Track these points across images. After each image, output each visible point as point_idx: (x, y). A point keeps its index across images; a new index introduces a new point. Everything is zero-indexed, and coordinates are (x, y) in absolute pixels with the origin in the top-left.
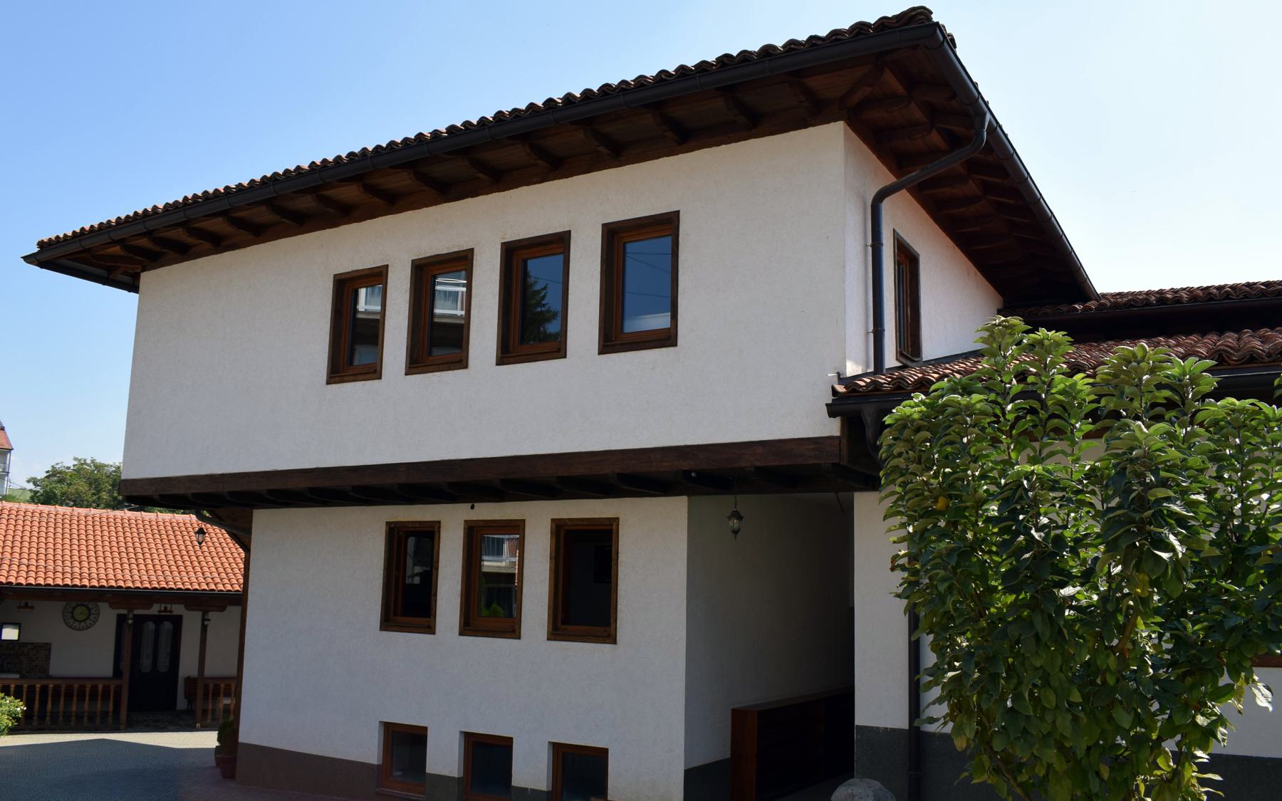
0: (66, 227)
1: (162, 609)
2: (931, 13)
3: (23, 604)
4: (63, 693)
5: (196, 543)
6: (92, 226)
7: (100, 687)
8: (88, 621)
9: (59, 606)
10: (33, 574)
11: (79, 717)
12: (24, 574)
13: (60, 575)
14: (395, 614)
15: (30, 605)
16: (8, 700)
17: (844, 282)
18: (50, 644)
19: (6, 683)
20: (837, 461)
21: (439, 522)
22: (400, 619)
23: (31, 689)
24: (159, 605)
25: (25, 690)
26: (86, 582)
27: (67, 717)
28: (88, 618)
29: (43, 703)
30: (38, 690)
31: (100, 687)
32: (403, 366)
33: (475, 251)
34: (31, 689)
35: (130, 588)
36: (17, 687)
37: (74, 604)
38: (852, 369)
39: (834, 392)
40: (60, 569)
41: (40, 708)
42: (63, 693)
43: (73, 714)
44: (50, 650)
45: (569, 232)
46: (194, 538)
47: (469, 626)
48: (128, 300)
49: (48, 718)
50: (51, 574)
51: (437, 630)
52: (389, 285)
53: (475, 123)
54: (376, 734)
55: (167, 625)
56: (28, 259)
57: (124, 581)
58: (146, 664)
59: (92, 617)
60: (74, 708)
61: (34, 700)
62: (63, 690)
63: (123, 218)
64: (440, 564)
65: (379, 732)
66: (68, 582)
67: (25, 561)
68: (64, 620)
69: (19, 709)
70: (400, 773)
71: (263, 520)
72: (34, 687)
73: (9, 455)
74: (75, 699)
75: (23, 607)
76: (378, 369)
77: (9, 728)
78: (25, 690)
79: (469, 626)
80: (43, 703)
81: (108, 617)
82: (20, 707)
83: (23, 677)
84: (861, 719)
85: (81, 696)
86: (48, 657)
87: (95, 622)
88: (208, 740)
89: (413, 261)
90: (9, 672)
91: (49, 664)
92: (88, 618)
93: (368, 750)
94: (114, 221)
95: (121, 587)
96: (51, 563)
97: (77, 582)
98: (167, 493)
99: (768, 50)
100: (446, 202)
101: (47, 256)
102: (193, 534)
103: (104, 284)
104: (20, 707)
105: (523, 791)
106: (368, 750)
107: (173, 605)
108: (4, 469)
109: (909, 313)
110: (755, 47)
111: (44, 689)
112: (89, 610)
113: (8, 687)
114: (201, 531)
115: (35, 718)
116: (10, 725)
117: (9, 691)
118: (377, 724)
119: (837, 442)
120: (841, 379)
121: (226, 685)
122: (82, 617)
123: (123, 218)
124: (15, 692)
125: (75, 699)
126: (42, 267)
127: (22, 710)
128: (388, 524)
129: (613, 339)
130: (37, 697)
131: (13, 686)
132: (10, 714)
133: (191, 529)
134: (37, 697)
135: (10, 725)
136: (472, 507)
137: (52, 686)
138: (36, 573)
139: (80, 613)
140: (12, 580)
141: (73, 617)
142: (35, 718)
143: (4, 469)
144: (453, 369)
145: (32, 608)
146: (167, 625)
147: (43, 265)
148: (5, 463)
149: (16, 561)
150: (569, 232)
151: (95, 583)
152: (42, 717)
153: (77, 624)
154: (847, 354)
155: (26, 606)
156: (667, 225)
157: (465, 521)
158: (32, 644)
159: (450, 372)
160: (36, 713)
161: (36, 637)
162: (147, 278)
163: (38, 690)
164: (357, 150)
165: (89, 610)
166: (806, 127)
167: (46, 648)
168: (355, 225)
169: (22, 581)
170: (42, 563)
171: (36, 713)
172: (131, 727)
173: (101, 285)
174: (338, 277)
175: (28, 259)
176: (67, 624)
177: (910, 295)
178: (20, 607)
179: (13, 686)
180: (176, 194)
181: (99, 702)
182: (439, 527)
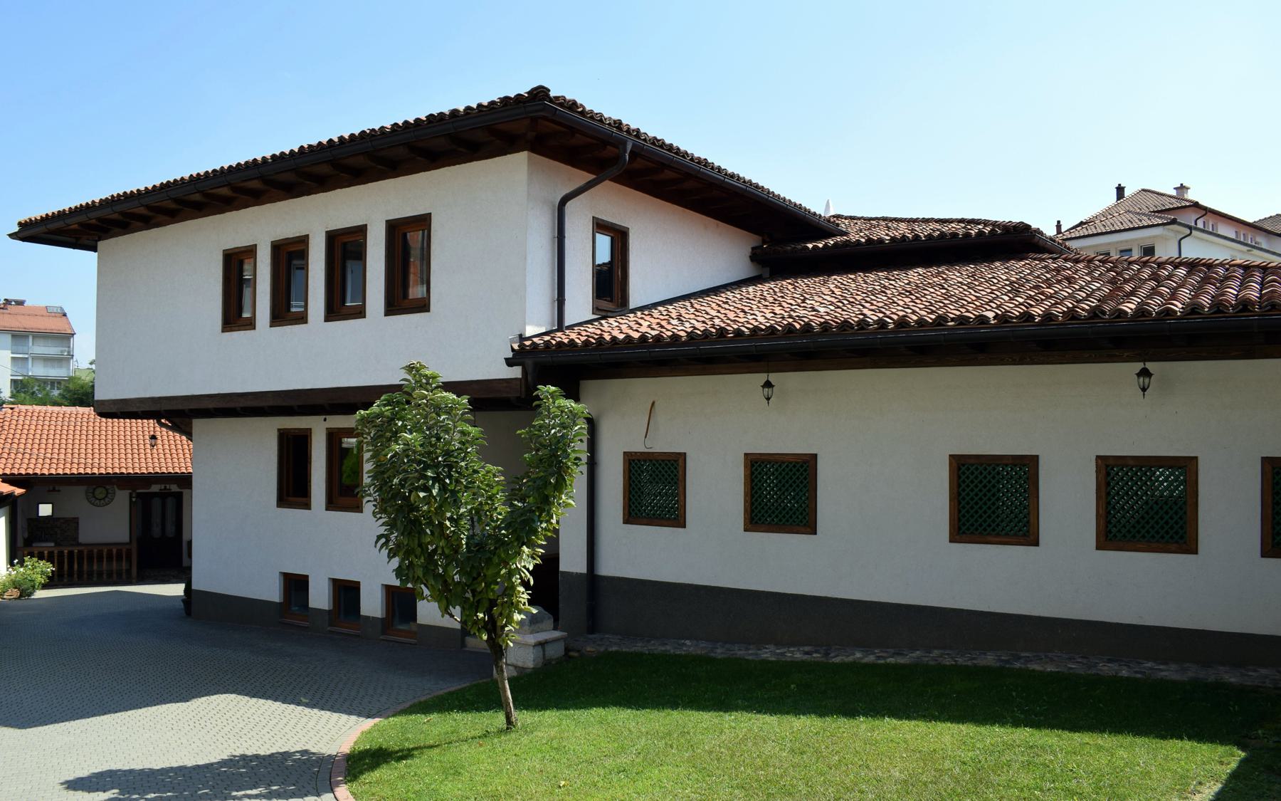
0: (37, 212)
1: (163, 488)
2: (549, 91)
3: (51, 488)
4: (105, 556)
5: (148, 446)
6: (53, 213)
7: (115, 551)
8: (106, 500)
9: (81, 489)
10: (54, 466)
11: (100, 574)
12: (47, 466)
13: (75, 466)
14: (288, 496)
15: (57, 489)
16: (42, 563)
17: (525, 269)
18: (78, 518)
19: (41, 550)
20: (519, 395)
21: (311, 429)
22: (291, 499)
23: (61, 554)
24: (765, 375)
25: (56, 555)
26: (95, 471)
27: (90, 574)
28: (106, 497)
29: (80, 565)
30: (66, 554)
31: (115, 551)
32: (269, 320)
33: (310, 237)
34: (61, 554)
35: (130, 473)
36: (49, 553)
37: (94, 487)
38: (530, 331)
39: (513, 350)
40: (75, 460)
41: (68, 569)
42: (105, 556)
43: (105, 572)
44: (78, 523)
45: (366, 225)
46: (148, 442)
47: (332, 504)
48: (92, 256)
49: (76, 576)
50: (68, 465)
51: (312, 507)
52: (258, 260)
53: (287, 153)
54: (278, 582)
55: (170, 502)
56: (12, 236)
57: (126, 468)
58: (156, 531)
59: (109, 496)
60: (95, 567)
61: (64, 562)
62: (85, 553)
63: (73, 208)
64: (312, 460)
65: (329, 585)
66: (82, 471)
67: (49, 455)
68: (87, 499)
69: (49, 570)
70: (297, 608)
71: (198, 425)
72: (62, 552)
73: (72, 339)
74: (95, 560)
75: (52, 491)
76: (253, 322)
77: (43, 584)
78: (56, 555)
79: (332, 504)
80: (80, 565)
81: (122, 498)
82: (49, 568)
83: (57, 544)
84: (563, 568)
85: (100, 559)
86: (77, 528)
87: (112, 499)
88: (177, 590)
89: (272, 242)
90: (47, 541)
91: (78, 534)
92: (106, 497)
93: (272, 592)
94: (67, 210)
95: (123, 473)
96: (69, 456)
97: (89, 471)
98: (125, 410)
99: (454, 113)
100: (291, 198)
101: (27, 233)
102: (147, 437)
103: (74, 249)
104: (49, 568)
105: (367, 618)
106: (272, 592)
107: (770, 374)
108: (69, 352)
109: (620, 273)
110: (446, 110)
111: (71, 554)
112: (107, 490)
113: (43, 553)
114: (153, 437)
115: (66, 576)
116: (43, 582)
117: (44, 556)
118: (278, 574)
119: (519, 382)
120: (522, 338)
121: (117, 550)
122: (102, 496)
123: (73, 208)
124: (48, 556)
125: (95, 560)
126: (23, 241)
127: (52, 570)
128: (279, 430)
129: (396, 304)
130: (66, 560)
131: (46, 552)
132: (43, 573)
133: (147, 433)
134: (66, 560)
135: (43, 582)
136: (325, 420)
137: (76, 551)
138: (57, 464)
139: (100, 492)
140: (38, 471)
141: (93, 493)
142: (66, 576)
143: (69, 352)
144: (299, 324)
145: (59, 491)
146: (170, 502)
147: (24, 239)
148: (69, 347)
149: (42, 456)
150: (366, 225)
151: (103, 471)
152: (71, 574)
153: (98, 501)
154: (527, 321)
155: (54, 490)
156: (423, 222)
157: (327, 429)
158: (63, 518)
159: (297, 326)
160: (66, 573)
161: (68, 514)
162: (101, 244)
163: (66, 554)
164: (218, 168)
165: (107, 490)
166: (505, 154)
167: (75, 521)
168: (234, 212)
169: (46, 472)
170: (62, 456)
171: (66, 573)
172: (142, 580)
173: (72, 249)
174: (227, 252)
175: (12, 236)
176: (90, 502)
177: (621, 260)
178: (49, 491)
179: (46, 552)
180: (105, 194)
181: (105, 563)
182: (311, 433)
